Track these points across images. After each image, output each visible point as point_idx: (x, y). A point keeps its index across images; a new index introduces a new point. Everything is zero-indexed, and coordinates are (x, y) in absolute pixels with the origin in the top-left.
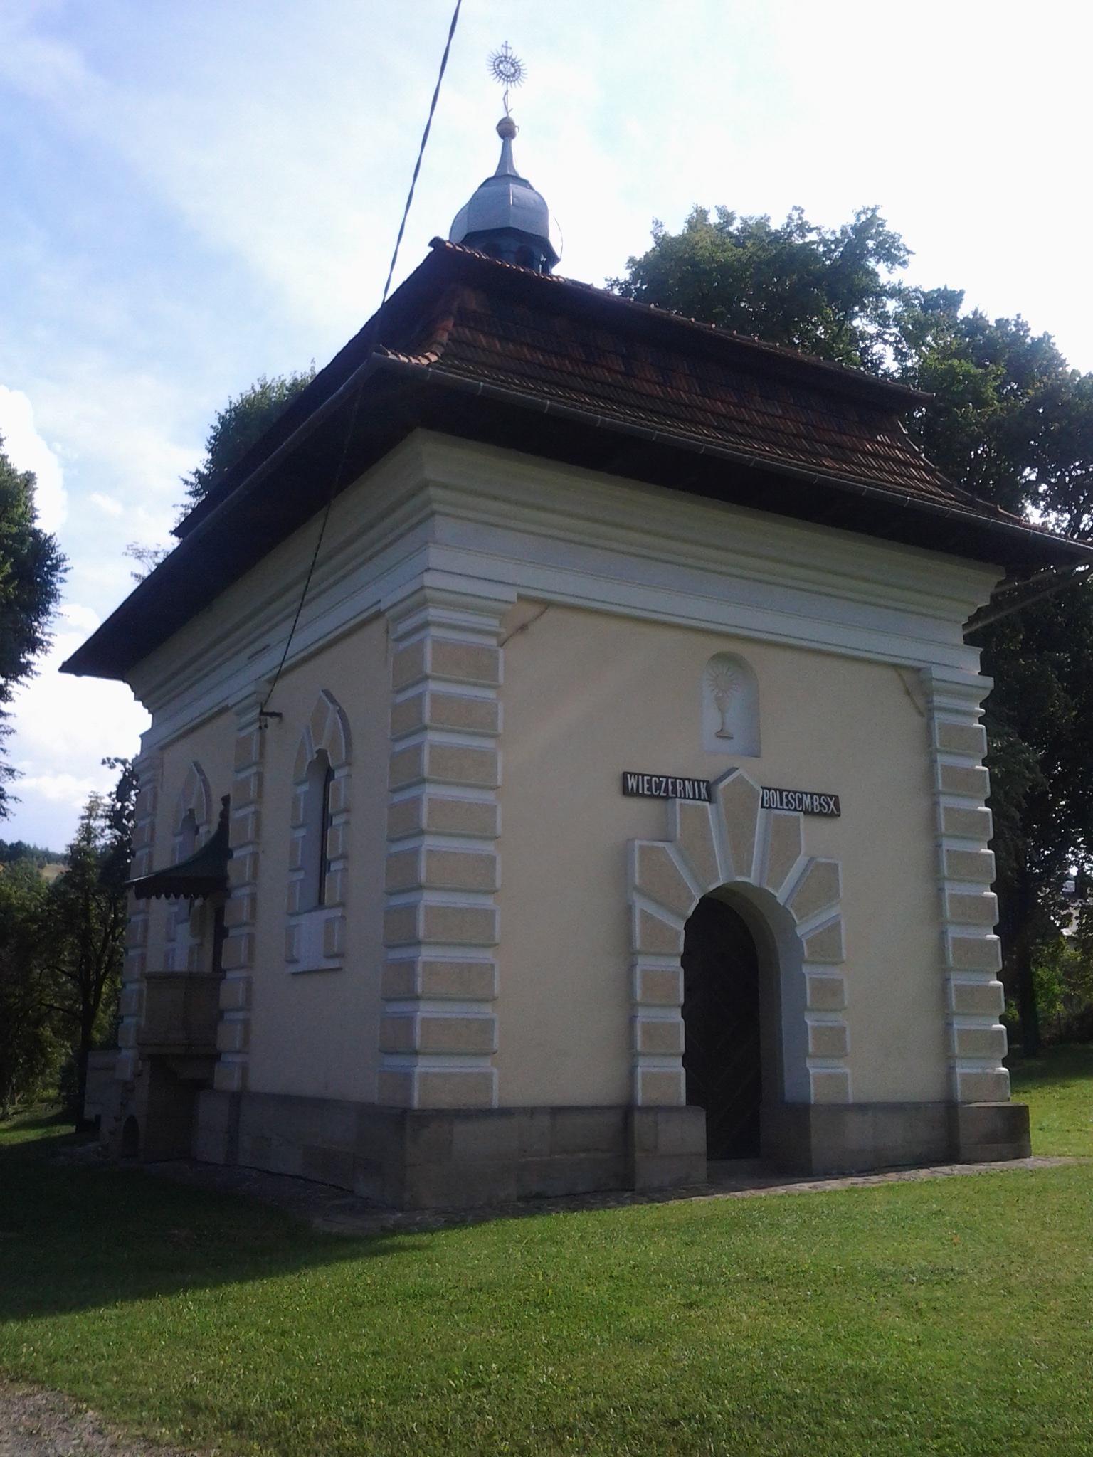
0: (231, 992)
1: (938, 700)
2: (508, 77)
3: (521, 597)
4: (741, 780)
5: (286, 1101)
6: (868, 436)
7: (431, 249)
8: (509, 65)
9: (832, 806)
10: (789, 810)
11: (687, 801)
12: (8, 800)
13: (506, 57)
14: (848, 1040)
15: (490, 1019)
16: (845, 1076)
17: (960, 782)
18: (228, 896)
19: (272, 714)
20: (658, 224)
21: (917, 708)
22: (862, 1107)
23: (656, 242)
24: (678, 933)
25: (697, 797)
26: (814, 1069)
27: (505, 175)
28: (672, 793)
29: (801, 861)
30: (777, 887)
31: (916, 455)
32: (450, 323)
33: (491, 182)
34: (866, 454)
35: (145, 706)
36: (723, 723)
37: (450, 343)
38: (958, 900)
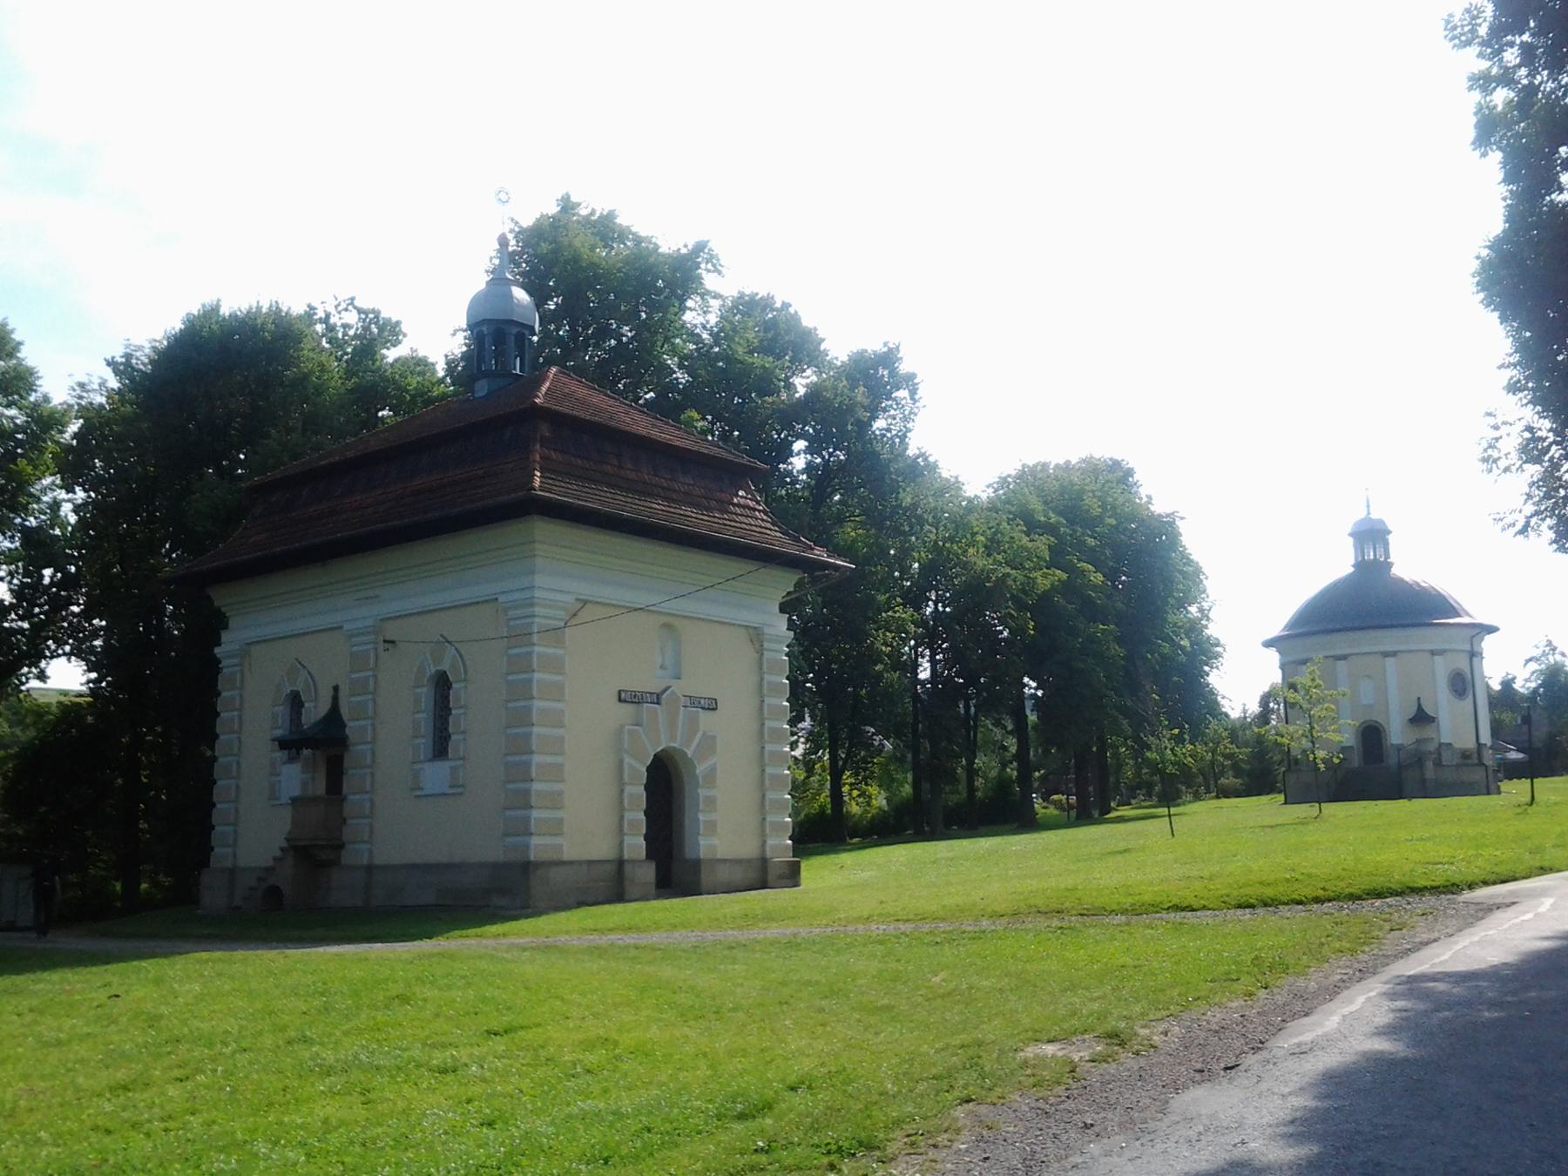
1: (766, 645)
26: (703, 842)
29: (699, 735)
31: (758, 503)
32: (538, 447)
38: (772, 753)
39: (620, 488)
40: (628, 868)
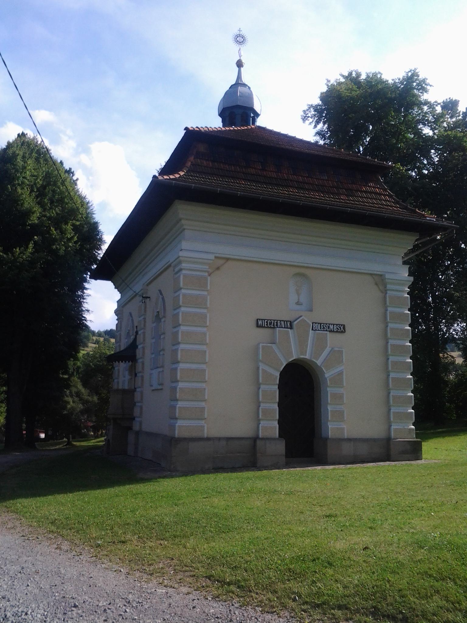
0: (137, 396)
1: (389, 286)
2: (240, 43)
3: (215, 257)
4: (304, 321)
5: (150, 434)
6: (365, 184)
7: (186, 131)
8: (241, 38)
9: (342, 329)
10: (324, 331)
11: (281, 329)
12: (88, 321)
13: (240, 35)
14: (345, 415)
15: (203, 407)
16: (343, 429)
17: (399, 317)
18: (137, 362)
19: (147, 297)
20: (328, 81)
21: (380, 290)
22: (349, 440)
23: (328, 87)
24: (276, 377)
25: (286, 327)
26: (331, 426)
27: (239, 83)
28: (276, 326)
29: (328, 350)
30: (317, 360)
31: (385, 190)
33: (233, 87)
34: (361, 192)
35: (118, 291)
36: (299, 299)
37: (191, 166)
38: (395, 363)
39: (282, 186)
40: (259, 443)
